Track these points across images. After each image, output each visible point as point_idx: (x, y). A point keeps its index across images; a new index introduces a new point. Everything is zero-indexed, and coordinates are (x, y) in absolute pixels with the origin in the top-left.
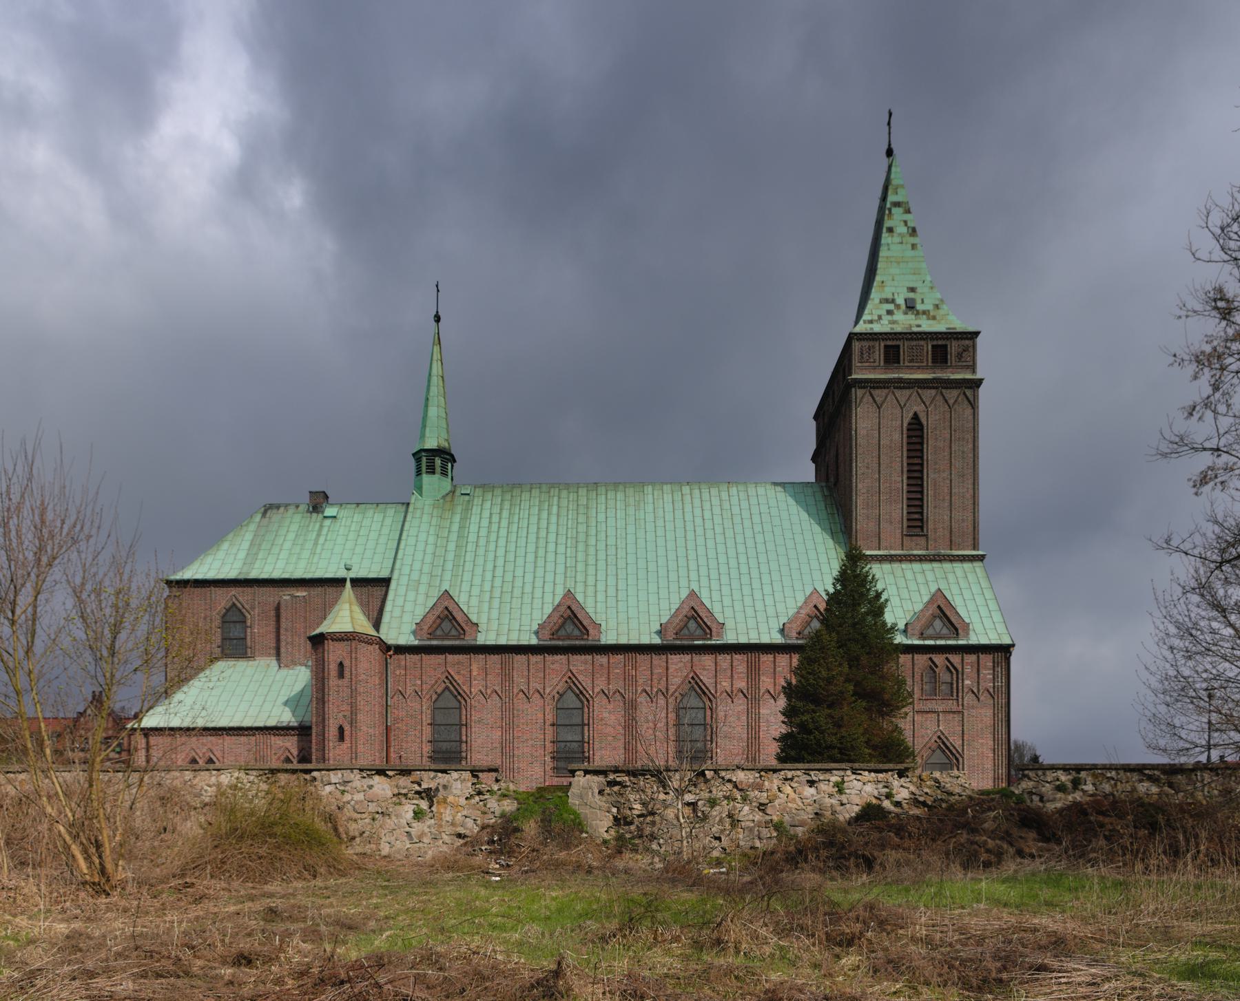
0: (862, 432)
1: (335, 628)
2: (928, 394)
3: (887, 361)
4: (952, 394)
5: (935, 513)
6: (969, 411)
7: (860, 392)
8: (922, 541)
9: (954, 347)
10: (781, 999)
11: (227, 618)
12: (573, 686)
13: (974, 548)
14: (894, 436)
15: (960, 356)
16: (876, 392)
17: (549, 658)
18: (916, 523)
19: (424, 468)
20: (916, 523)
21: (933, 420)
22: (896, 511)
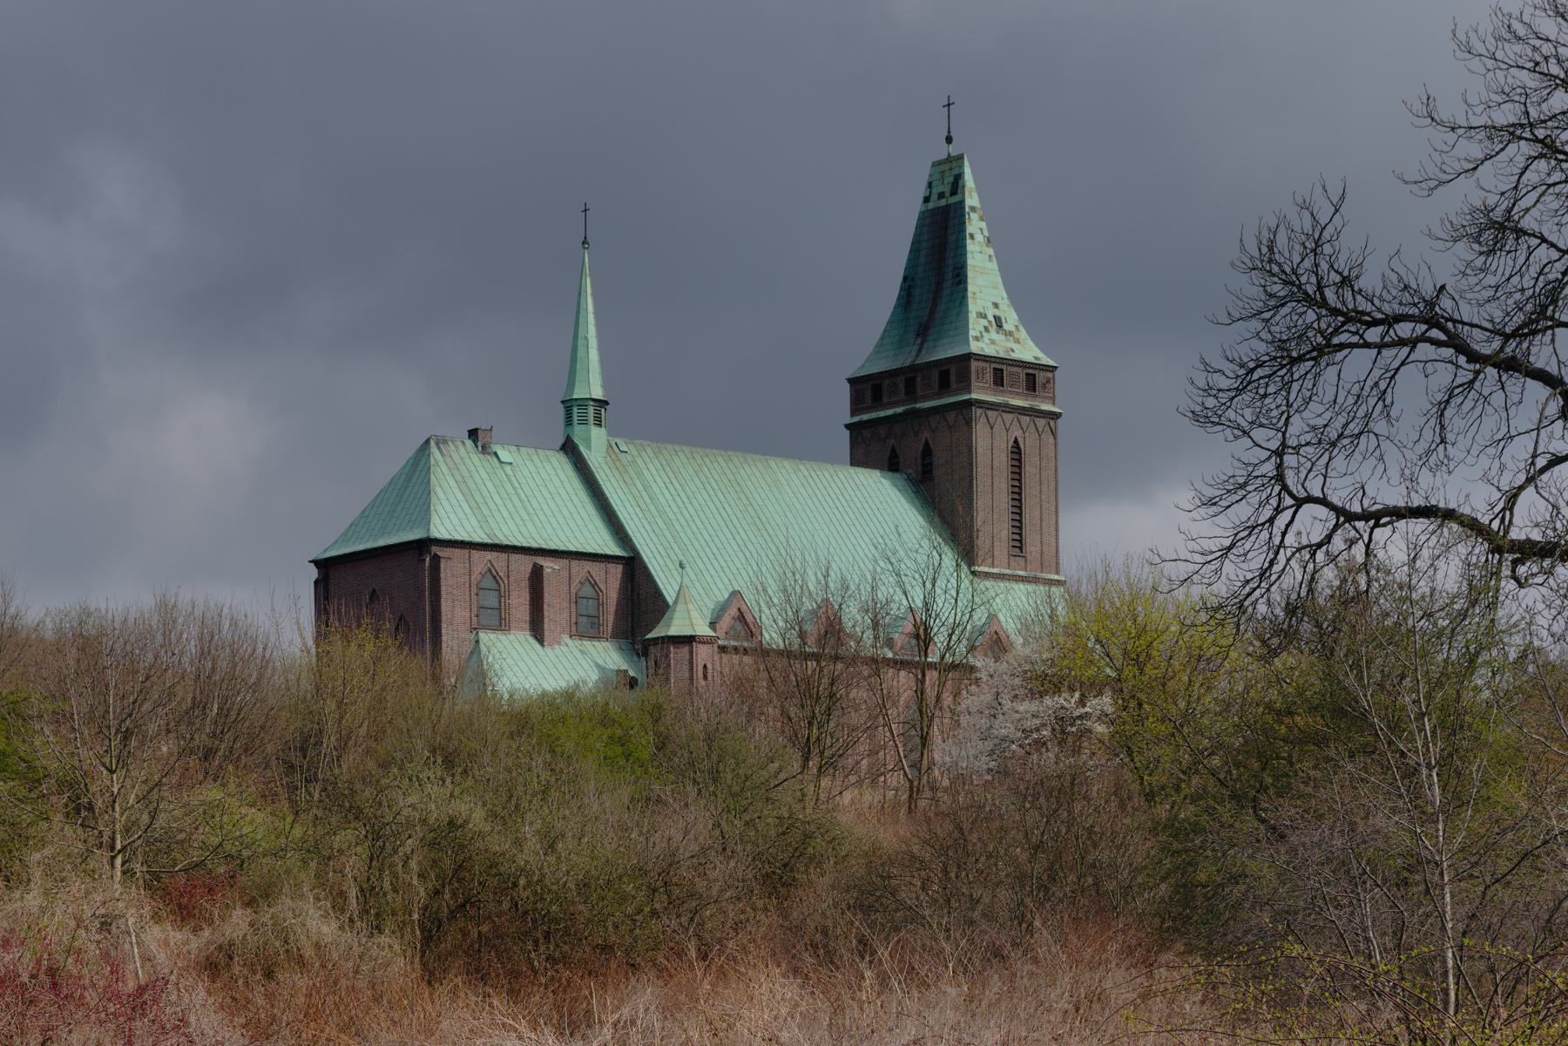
0: (980, 450)
1: (673, 631)
2: (1025, 420)
3: (996, 383)
4: (1041, 422)
5: (1032, 547)
6: (1052, 440)
7: (979, 411)
8: (1021, 561)
9: (1041, 377)
10: (14, 880)
11: (483, 585)
12: (535, 565)
13: (1057, 573)
14: (1003, 460)
15: (1044, 386)
16: (990, 413)
17: (574, 563)
18: (1018, 544)
19: (575, 421)
20: (1018, 544)
21: (1028, 446)
22: (1004, 531)
